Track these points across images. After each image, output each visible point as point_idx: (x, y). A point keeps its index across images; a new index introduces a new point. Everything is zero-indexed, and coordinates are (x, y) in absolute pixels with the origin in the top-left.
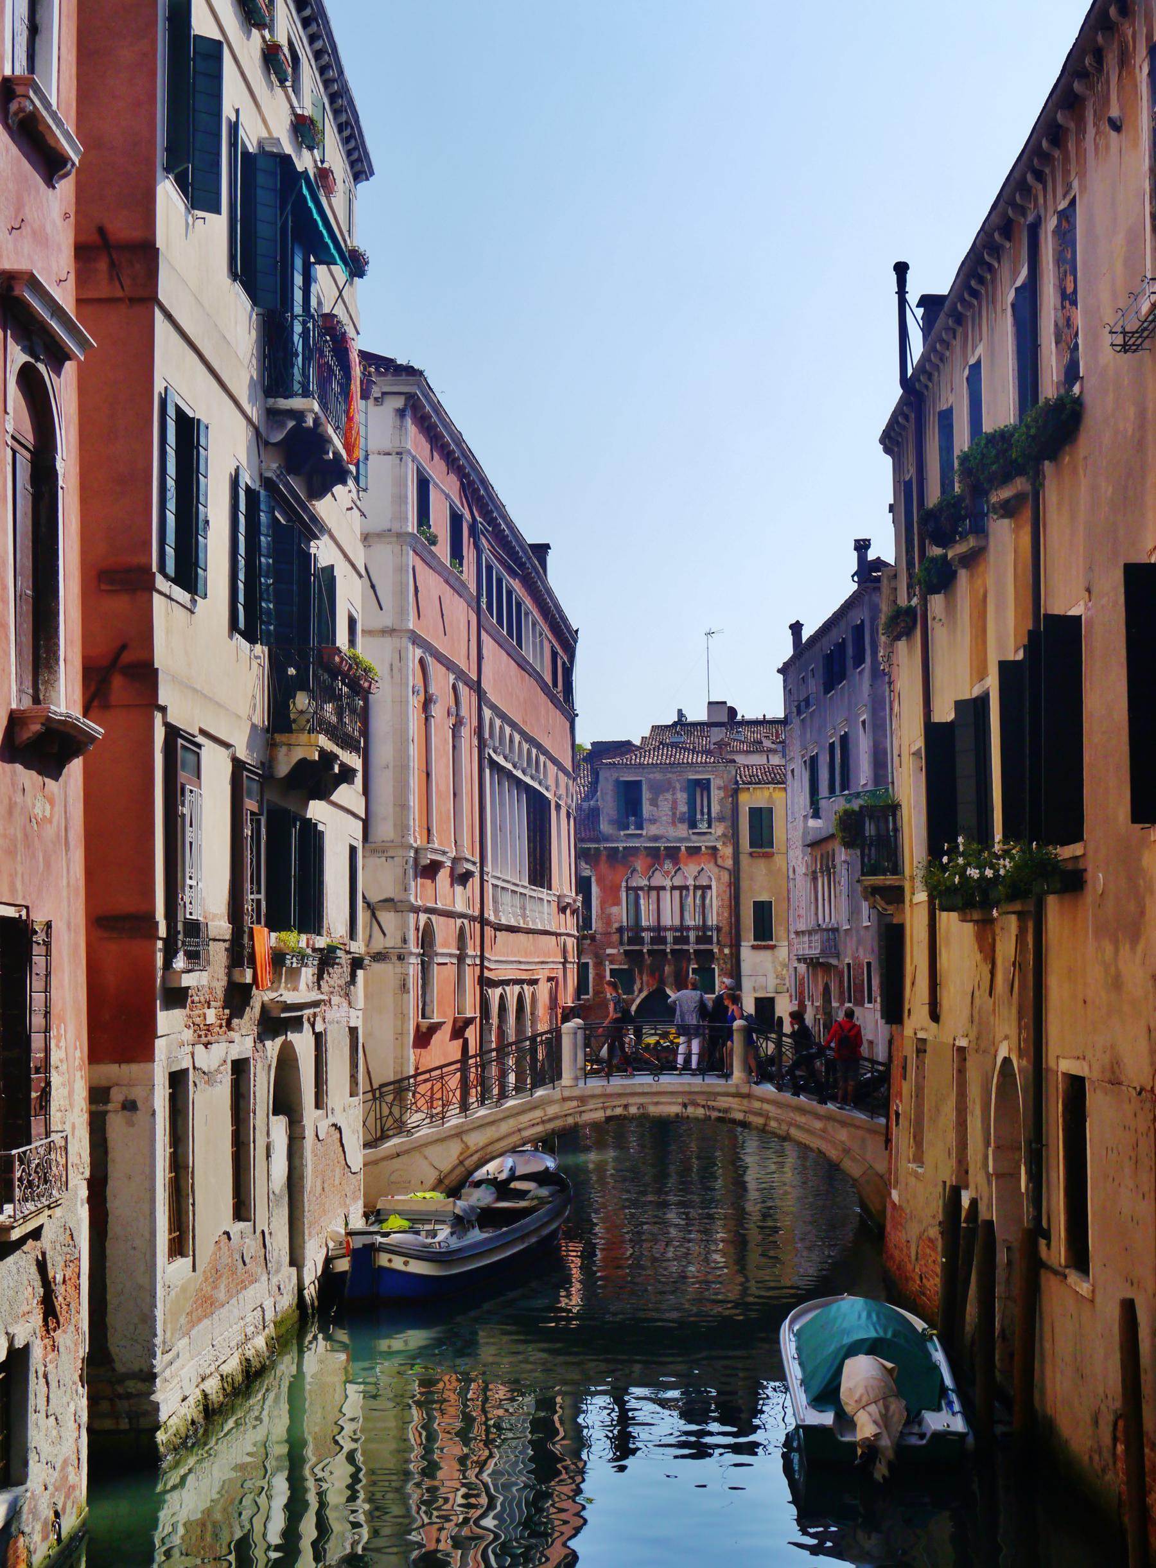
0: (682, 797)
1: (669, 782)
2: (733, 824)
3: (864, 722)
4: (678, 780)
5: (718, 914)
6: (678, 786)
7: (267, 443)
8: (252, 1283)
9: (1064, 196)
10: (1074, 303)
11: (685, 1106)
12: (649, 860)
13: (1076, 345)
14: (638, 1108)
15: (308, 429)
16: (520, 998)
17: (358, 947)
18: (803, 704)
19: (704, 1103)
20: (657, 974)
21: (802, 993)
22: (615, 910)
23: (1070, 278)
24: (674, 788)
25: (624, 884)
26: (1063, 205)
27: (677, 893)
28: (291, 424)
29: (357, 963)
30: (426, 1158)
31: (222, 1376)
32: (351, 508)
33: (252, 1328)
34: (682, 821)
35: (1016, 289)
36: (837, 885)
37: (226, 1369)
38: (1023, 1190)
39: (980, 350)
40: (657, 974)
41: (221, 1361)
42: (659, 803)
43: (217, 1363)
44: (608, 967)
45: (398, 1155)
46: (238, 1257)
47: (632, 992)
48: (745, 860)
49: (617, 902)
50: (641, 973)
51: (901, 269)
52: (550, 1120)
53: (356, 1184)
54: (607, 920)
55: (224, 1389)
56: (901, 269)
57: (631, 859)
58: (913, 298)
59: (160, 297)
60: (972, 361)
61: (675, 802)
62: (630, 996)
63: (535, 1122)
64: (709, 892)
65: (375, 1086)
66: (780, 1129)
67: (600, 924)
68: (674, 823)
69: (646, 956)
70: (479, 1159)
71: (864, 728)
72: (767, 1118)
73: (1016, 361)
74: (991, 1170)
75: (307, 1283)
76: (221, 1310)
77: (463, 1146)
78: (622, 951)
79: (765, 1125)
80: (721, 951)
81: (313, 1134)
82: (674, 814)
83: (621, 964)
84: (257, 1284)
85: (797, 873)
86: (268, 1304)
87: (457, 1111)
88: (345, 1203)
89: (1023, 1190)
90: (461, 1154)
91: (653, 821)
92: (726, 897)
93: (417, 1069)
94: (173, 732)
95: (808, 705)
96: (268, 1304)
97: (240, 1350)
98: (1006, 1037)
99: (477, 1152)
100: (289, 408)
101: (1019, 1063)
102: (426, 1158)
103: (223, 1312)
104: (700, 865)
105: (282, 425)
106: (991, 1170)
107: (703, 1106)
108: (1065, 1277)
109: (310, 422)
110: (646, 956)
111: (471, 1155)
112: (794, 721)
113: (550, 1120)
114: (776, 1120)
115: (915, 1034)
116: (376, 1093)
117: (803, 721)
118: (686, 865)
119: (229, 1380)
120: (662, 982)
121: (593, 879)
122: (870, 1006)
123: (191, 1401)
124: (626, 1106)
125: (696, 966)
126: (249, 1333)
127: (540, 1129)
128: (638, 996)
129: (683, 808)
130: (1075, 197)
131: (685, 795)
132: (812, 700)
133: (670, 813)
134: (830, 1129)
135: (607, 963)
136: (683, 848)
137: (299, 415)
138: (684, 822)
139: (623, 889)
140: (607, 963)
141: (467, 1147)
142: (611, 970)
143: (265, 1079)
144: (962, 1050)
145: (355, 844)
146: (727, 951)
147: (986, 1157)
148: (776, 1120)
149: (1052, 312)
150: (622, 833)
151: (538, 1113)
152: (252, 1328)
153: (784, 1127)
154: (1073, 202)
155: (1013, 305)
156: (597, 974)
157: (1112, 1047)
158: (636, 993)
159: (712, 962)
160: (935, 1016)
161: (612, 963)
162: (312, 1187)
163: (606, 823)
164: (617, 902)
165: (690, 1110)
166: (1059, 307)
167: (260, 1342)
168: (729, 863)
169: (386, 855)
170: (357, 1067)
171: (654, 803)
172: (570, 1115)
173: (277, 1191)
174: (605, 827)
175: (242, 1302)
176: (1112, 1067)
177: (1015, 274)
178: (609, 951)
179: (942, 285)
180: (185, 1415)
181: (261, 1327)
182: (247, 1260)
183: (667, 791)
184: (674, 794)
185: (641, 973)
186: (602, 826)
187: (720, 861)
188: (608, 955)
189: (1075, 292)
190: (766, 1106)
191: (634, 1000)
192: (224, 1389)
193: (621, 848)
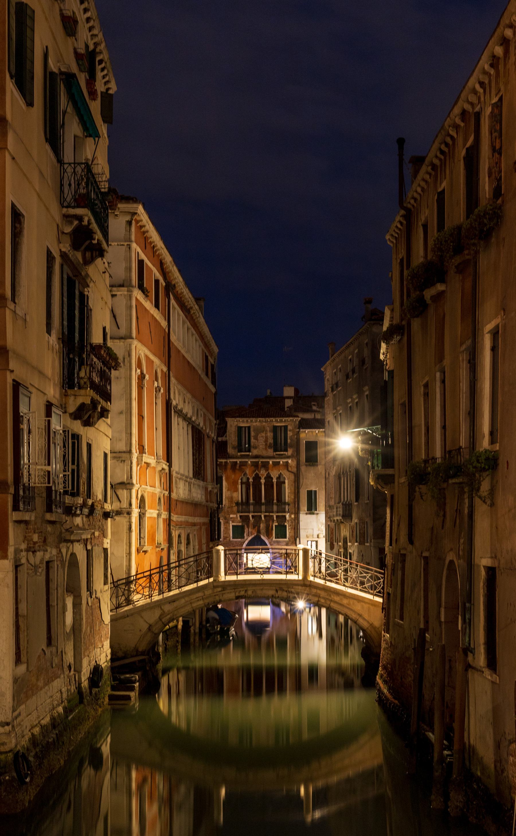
0: (270, 435)
1: (264, 427)
2: (297, 449)
3: (367, 395)
4: (268, 426)
5: (288, 497)
6: (268, 429)
7: (63, 233)
8: (56, 678)
9: (496, 95)
10: (500, 154)
11: (277, 591)
12: (253, 468)
13: (501, 177)
14: (253, 592)
15: (85, 226)
16: (179, 536)
17: (108, 507)
18: (335, 386)
19: (287, 589)
20: (256, 528)
21: (332, 538)
22: (235, 495)
23: (498, 141)
24: (266, 431)
25: (240, 481)
26: (495, 100)
27: (123, 331)
28: (76, 223)
29: (106, 515)
30: (142, 617)
31: (41, 726)
32: (104, 272)
33: (56, 702)
34: (270, 447)
35: (467, 149)
36: (351, 481)
37: (43, 722)
38: (460, 628)
39: (444, 184)
40: (256, 528)
41: (41, 718)
42: (258, 438)
43: (39, 719)
44: (231, 524)
45: (128, 616)
46: (49, 664)
47: (243, 537)
48: (303, 468)
49: (236, 490)
50: (248, 527)
51: (401, 142)
52: (207, 598)
53: (107, 631)
54: (231, 499)
55: (43, 733)
56: (401, 142)
57: (244, 467)
58: (407, 158)
59: (8, 148)
60: (440, 190)
61: (267, 438)
62: (243, 539)
63: (199, 599)
64: (283, 485)
65: (115, 580)
66: (326, 603)
67: (227, 502)
68: (266, 449)
69: (251, 519)
70: (170, 618)
71: (367, 398)
72: (319, 597)
73: (465, 189)
74: (443, 619)
75: (83, 680)
76: (41, 692)
77: (162, 611)
78: (238, 516)
79: (318, 601)
80: (290, 516)
81: (86, 602)
82: (266, 445)
83: (238, 523)
84: (58, 679)
85: (330, 476)
86: (64, 690)
87: (157, 594)
88: (101, 640)
89: (460, 628)
90: (161, 615)
91: (256, 448)
92: (293, 489)
93: (137, 571)
94: (16, 386)
95: (337, 387)
96: (64, 690)
97: (50, 713)
98: (451, 550)
99: (169, 614)
100: (74, 213)
101: (458, 562)
102: (142, 617)
103: (42, 692)
104: (279, 471)
105: (71, 223)
106: (443, 619)
107: (286, 591)
108: (483, 672)
109: (85, 223)
110: (251, 519)
111: (166, 616)
112: (330, 395)
113: (207, 598)
114: (324, 598)
115: (400, 551)
116: (116, 585)
117: (334, 395)
118: (272, 470)
119: (45, 728)
120: (259, 532)
121: (224, 478)
122: (368, 544)
123: (27, 738)
124: (246, 591)
125: (277, 524)
126: (55, 705)
127: (201, 602)
128: (247, 539)
129: (271, 441)
130: (502, 96)
131: (272, 434)
132: (340, 384)
133: (264, 444)
134: (351, 603)
135: (231, 522)
136: (271, 463)
137: (80, 218)
138: (271, 448)
139: (239, 483)
140: (231, 522)
141: (164, 611)
142: (233, 526)
143: (62, 574)
144: (426, 558)
145: (107, 452)
146: (293, 516)
147: (439, 613)
148: (324, 598)
149: (487, 160)
150: (239, 454)
151: (200, 594)
152: (56, 702)
153: (328, 602)
154: (501, 99)
155: (464, 158)
156: (225, 528)
157: (512, 550)
158: (246, 538)
159: (285, 522)
160: (411, 541)
161: (233, 522)
162: (85, 631)
163: (231, 448)
164: (236, 490)
165: (279, 593)
166: (491, 156)
167: (60, 709)
168: (295, 470)
169: (121, 459)
170: (107, 569)
171: (256, 438)
172: (217, 595)
173: (68, 631)
174: (230, 451)
175: (51, 688)
176: (512, 561)
177: (466, 140)
178: (231, 516)
179: (83, 366)
180: (24, 745)
181: (60, 702)
182: (54, 665)
183: (263, 432)
184: (266, 434)
185: (248, 527)
186: (228, 450)
187: (290, 469)
188: (231, 518)
189: (501, 148)
190: (319, 592)
191: (244, 542)
192: (43, 733)
193: (238, 462)
